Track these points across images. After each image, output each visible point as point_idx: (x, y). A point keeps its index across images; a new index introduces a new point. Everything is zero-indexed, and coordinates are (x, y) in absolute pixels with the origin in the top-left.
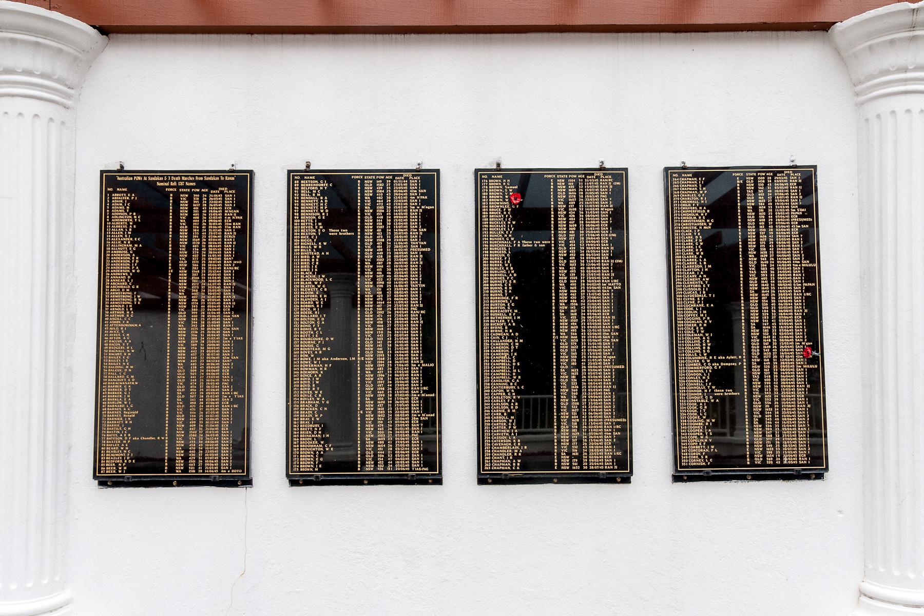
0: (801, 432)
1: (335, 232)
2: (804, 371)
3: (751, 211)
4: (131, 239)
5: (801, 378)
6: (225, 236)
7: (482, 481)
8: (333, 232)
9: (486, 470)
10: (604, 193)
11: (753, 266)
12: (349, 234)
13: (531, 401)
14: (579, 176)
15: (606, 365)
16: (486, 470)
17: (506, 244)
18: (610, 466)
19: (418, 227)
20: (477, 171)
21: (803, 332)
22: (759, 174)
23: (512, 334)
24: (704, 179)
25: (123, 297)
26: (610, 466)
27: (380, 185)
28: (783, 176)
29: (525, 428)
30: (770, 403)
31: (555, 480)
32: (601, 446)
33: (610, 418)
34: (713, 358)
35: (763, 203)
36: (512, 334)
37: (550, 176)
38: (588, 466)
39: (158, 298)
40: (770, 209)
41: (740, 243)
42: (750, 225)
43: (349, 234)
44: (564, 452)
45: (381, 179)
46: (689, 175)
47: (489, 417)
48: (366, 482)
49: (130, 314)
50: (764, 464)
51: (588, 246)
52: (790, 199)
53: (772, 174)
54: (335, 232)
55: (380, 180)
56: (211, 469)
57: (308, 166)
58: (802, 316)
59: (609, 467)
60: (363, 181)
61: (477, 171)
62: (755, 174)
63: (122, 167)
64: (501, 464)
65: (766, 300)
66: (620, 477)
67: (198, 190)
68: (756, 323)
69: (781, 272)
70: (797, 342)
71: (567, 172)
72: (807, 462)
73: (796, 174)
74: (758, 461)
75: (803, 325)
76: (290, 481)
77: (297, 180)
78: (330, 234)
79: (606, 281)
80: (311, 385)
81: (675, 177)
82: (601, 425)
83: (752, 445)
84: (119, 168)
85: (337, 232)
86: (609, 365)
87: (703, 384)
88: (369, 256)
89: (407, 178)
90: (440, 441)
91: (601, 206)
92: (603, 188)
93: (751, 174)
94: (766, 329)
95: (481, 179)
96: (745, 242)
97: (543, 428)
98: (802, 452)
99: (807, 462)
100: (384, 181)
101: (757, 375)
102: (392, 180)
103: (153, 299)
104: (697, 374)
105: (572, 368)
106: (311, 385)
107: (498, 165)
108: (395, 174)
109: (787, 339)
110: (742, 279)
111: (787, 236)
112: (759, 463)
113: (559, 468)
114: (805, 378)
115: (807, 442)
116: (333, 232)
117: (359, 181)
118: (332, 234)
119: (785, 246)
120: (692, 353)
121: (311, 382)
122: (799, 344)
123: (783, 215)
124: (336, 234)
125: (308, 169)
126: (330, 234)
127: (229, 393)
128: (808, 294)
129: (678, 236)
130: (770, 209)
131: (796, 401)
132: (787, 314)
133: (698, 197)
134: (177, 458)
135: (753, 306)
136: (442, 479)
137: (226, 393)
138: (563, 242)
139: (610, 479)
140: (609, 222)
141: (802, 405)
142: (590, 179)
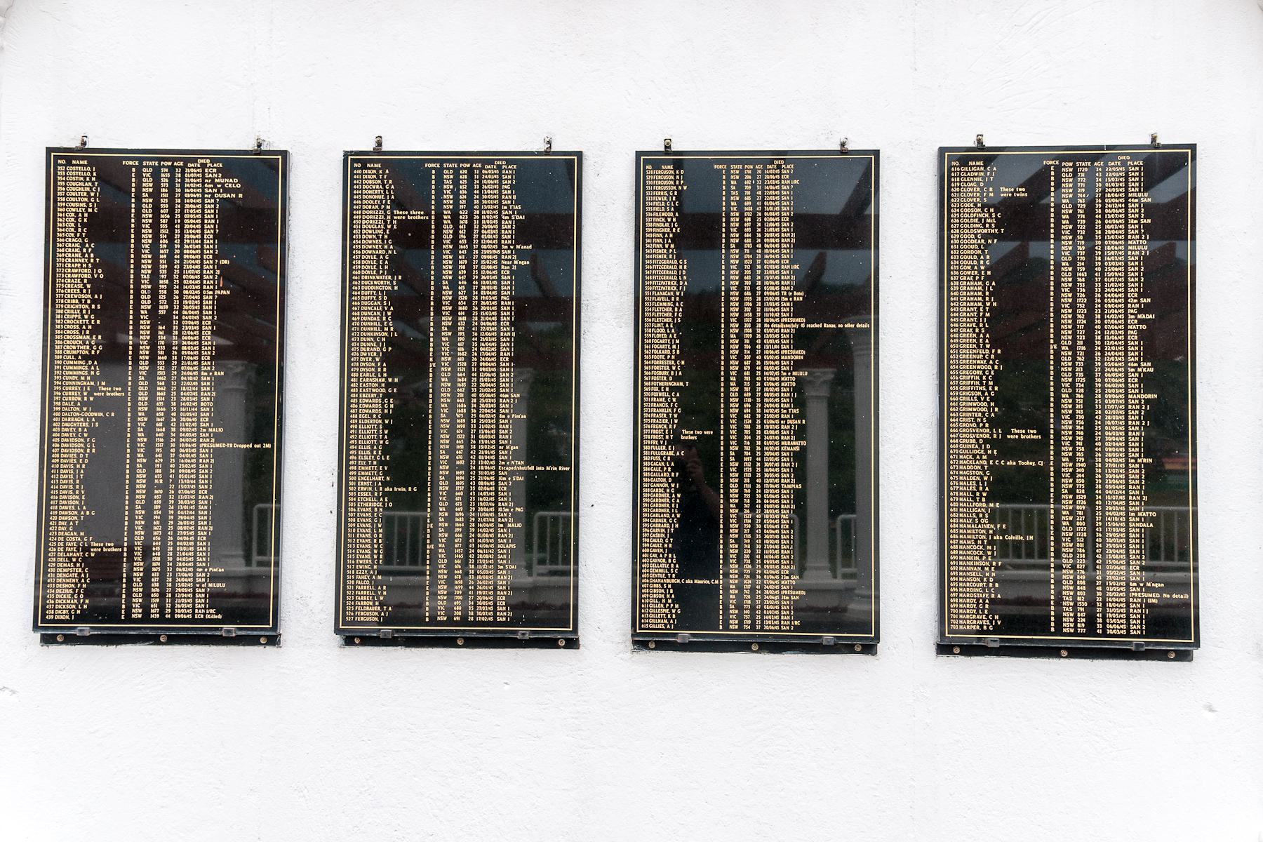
14: (474, 166)
20: (942, 151)
22: (162, 163)
24: (387, 171)
25: (76, 340)
27: (165, 176)
29: (410, 564)
31: (755, 647)
37: (130, 163)
38: (762, 625)
39: (228, 343)
45: (167, 167)
46: (82, 162)
49: (95, 371)
53: (182, 164)
55: (465, 169)
57: (84, 143)
60: (1058, 169)
61: (942, 151)
62: (157, 164)
63: (980, 142)
71: (460, 158)
72: (1142, 633)
73: (215, 165)
77: (61, 165)
80: (75, 481)
81: (61, 165)
84: (662, 149)
89: (499, 167)
90: (277, 578)
99: (1142, 633)
100: (172, 169)
102: (183, 169)
103: (225, 346)
104: (971, 478)
105: (457, 470)
106: (75, 481)
107: (1154, 139)
108: (187, 157)
113: (726, 628)
117: (134, 170)
121: (75, 476)
125: (83, 148)
134: (731, 587)
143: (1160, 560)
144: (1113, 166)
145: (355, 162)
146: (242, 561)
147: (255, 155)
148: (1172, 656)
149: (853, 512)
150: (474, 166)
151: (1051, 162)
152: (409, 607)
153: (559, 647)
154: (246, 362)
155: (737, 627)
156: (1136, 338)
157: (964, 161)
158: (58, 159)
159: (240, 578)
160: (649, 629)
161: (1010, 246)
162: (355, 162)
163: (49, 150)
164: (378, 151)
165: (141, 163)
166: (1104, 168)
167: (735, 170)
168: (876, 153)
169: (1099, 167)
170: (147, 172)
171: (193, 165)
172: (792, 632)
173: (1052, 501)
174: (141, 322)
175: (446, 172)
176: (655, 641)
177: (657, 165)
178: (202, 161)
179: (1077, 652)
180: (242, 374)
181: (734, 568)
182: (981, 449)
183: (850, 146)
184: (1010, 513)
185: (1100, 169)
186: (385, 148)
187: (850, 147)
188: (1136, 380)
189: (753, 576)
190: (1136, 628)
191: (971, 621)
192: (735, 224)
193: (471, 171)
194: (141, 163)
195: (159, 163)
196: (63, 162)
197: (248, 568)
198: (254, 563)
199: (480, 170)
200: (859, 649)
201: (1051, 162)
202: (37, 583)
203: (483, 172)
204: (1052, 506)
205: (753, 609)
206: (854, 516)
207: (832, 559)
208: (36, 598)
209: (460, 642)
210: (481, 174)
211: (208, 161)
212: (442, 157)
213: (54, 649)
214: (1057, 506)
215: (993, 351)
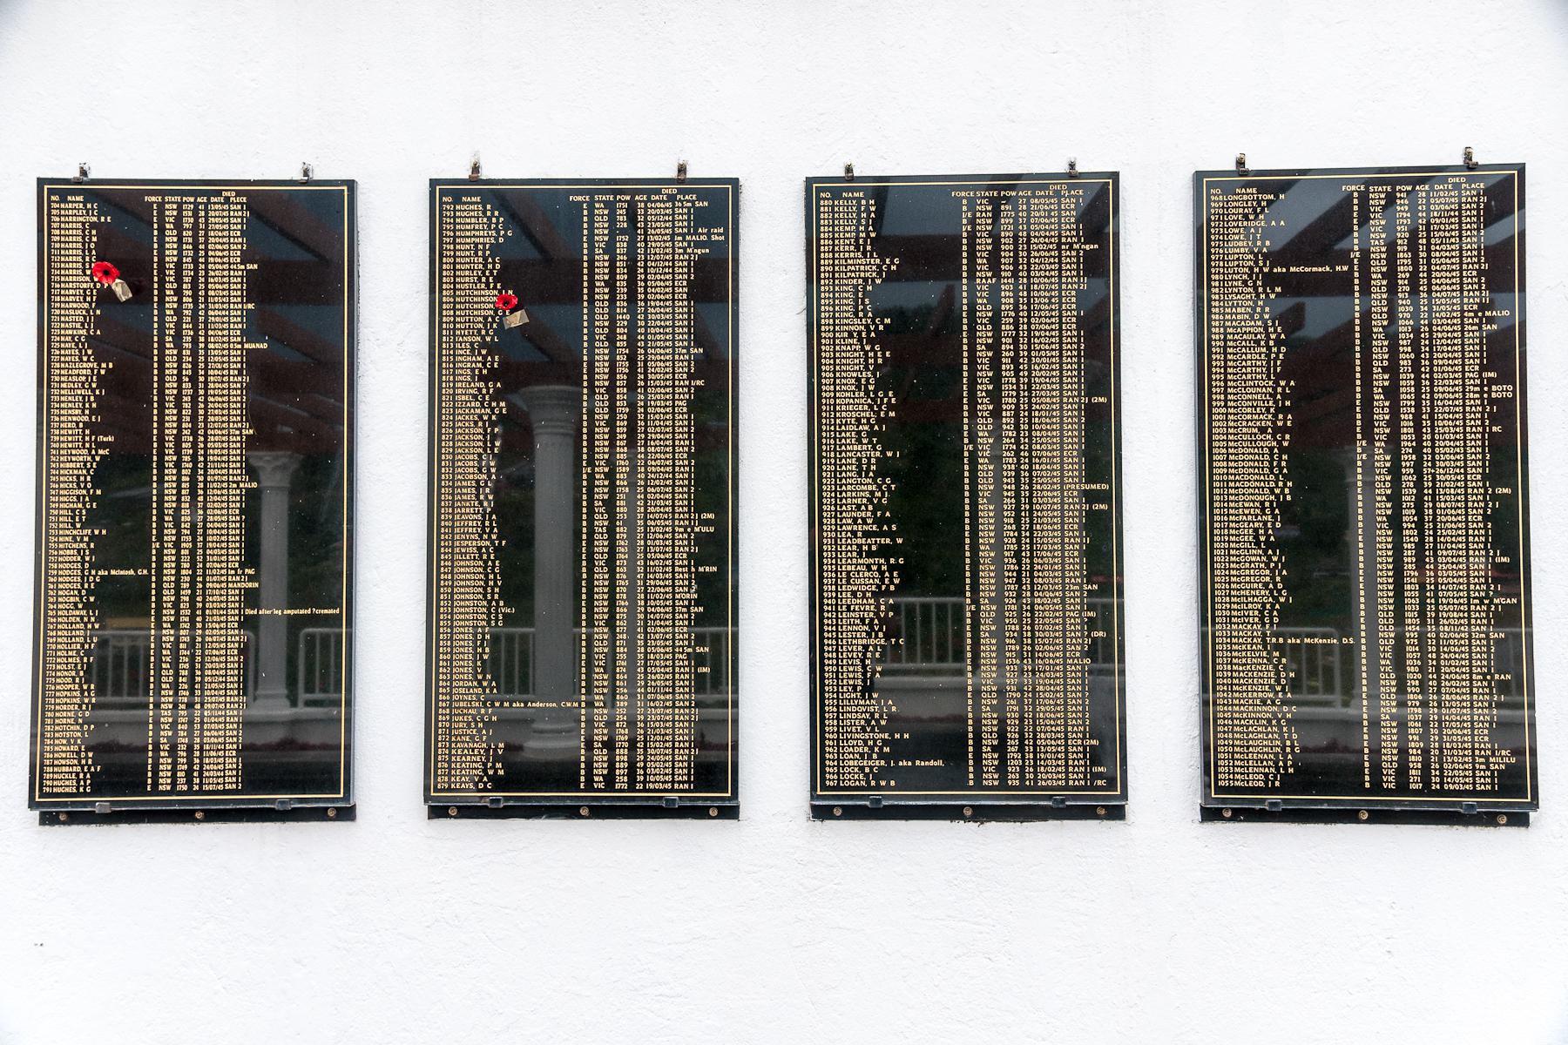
0: (1476, 566)
2: (1492, 777)
3: (1382, 397)
5: (1471, 224)
10: (1072, 607)
11: (1390, 772)
13: (918, 608)
14: (637, 198)
15: (1070, 483)
18: (1079, 780)
21: (1484, 460)
23: (876, 428)
26: (1079, 780)
28: (1449, 190)
29: (113, 695)
30: (1419, 663)
32: (1054, 257)
33: (1076, 483)
35: (1417, 749)
36: (876, 428)
41: (1357, 322)
42: (1384, 625)
44: (983, 497)
47: (834, 654)
48: (713, 812)
50: (1402, 788)
51: (1035, 383)
52: (1465, 433)
58: (1485, 515)
59: (1077, 783)
60: (1364, 197)
61: (809, 182)
64: (849, 274)
65: (1410, 333)
66: (1367, 810)
67: (192, 200)
68: (1383, 387)
69: (1447, 676)
70: (1474, 598)
72: (1493, 787)
73: (1473, 186)
74: (1389, 782)
75: (1483, 446)
76: (430, 807)
79: (1069, 240)
82: (1060, 712)
83: (1375, 724)
86: (1076, 483)
87: (1271, 395)
90: (349, 721)
91: (1063, 240)
92: (1071, 645)
93: (1380, 189)
94: (1410, 542)
95: (819, 199)
96: (1366, 316)
97: (943, 662)
98: (1471, 361)
99: (1493, 787)
101: (1379, 240)
109: (1451, 515)
110: (1359, 423)
111: (1458, 471)
112: (1391, 786)
114: (1481, 351)
115: (1487, 574)
119: (1451, 403)
120: (1251, 441)
122: (1480, 677)
123: (1450, 454)
128: (1494, 429)
129: (1219, 287)
131: (1461, 257)
133: (1268, 568)
135: (1384, 625)
136: (738, 807)
141: (1478, 502)
143: (947, 661)
145: (818, 192)
146: (287, 703)
149: (532, 625)
150: (637, 198)
151: (1353, 188)
152: (314, 747)
154: (289, 453)
156: (685, 410)
157: (457, 196)
158: (51, 192)
159: (283, 723)
162: (818, 192)
164: (474, 180)
165: (592, 198)
166: (206, 205)
168: (1115, 176)
170: (600, 210)
171: (657, 198)
174: (167, 411)
177: (457, 196)
178: (1453, 180)
180: (284, 468)
181: (167, 697)
183: (1081, 168)
184: (934, 608)
186: (690, 174)
187: (1079, 169)
188: (685, 456)
189: (190, 706)
191: (64, 781)
192: (602, 274)
194: (592, 198)
197: (294, 710)
198: (300, 703)
199: (206, 205)
201: (1353, 188)
202: (33, 736)
203: (649, 205)
205: (190, 749)
206: (532, 630)
207: (291, 681)
208: (33, 755)
210: (646, 209)
211: (1463, 180)
215: (93, 438)
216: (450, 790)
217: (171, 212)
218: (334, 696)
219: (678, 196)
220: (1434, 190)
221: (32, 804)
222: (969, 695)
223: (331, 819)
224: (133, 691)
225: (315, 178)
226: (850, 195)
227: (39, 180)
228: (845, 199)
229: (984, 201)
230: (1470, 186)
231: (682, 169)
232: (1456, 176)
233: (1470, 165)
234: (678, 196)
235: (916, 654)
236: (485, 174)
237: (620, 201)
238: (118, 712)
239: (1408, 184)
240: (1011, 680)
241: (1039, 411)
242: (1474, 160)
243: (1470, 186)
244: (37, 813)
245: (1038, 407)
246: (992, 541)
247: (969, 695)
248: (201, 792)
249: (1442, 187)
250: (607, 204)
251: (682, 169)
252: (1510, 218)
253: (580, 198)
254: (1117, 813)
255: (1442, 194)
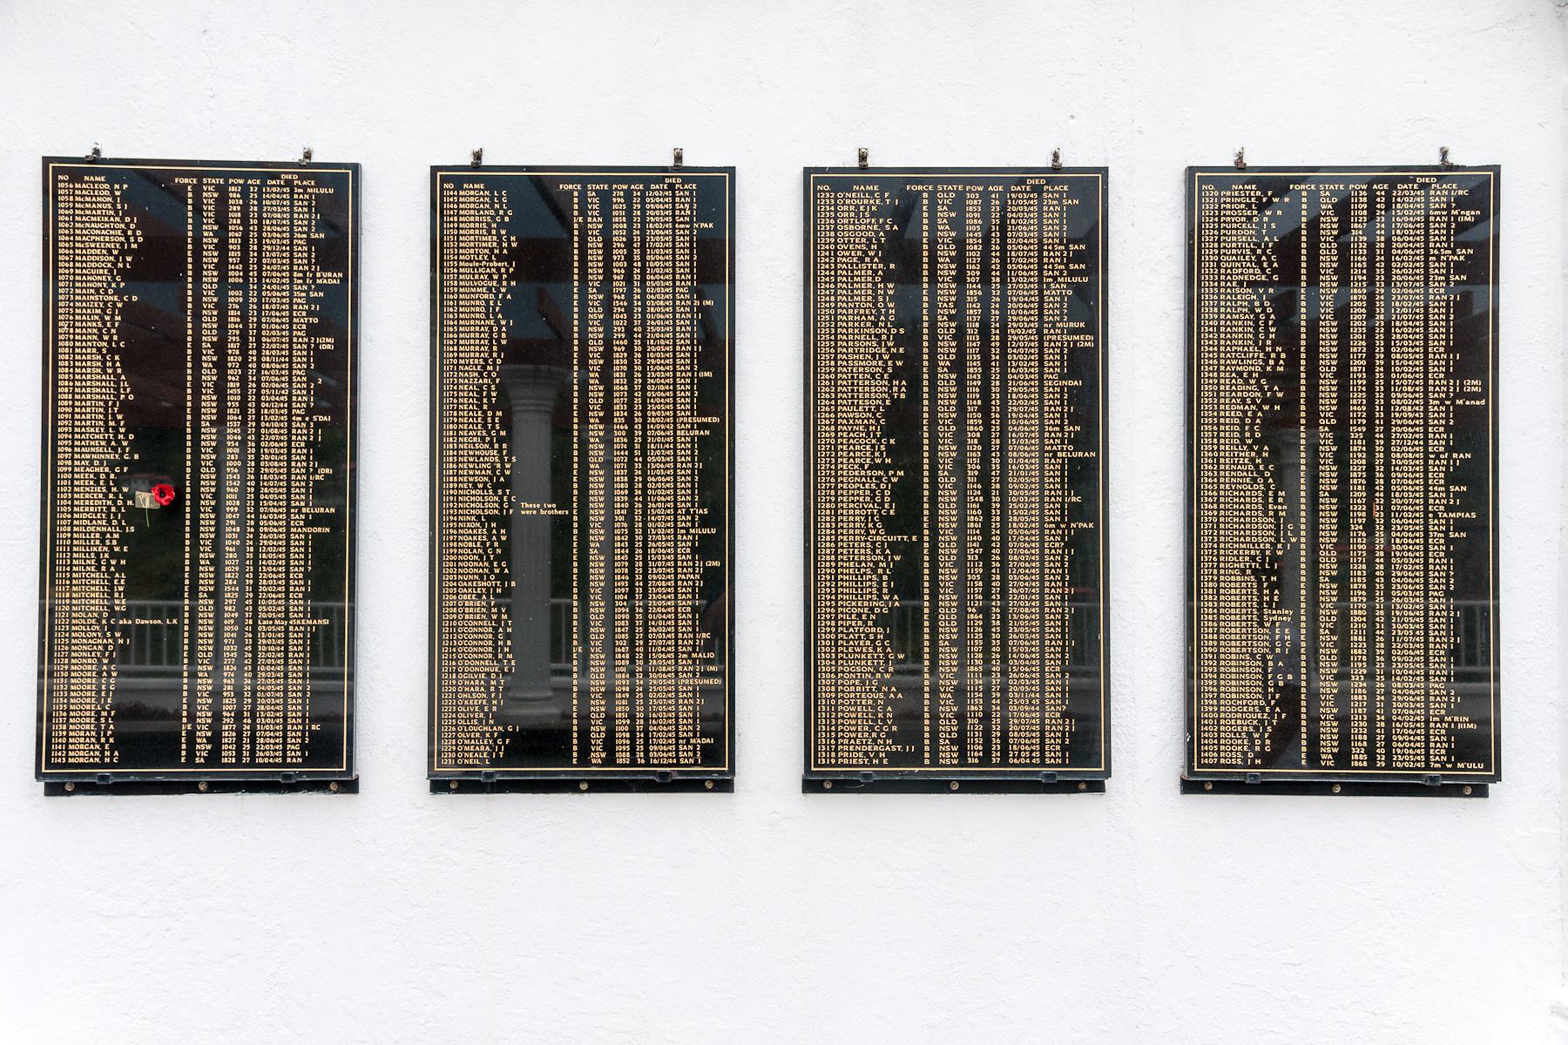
1: (533, 509)
4: (501, 728)
6: (1046, 544)
7: (812, 785)
8: (529, 509)
9: (1205, 766)
12: (560, 512)
16: (1205, 766)
17: (105, 394)
19: (1062, 422)
29: (324, 665)
34: (130, 298)
40: (995, 515)
43: (560, 512)
54: (533, 509)
56: (1408, 758)
61: (1191, 171)
63: (97, 151)
71: (227, 171)
73: (686, 187)
78: (523, 512)
85: (536, 509)
88: (209, 336)
93: (950, 187)
95: (56, 181)
105: (231, 290)
108: (266, 172)
116: (529, 509)
118: (527, 512)
124: (535, 512)
125: (96, 158)
126: (523, 512)
127: (307, 268)
130: (995, 515)
132: (1411, 245)
137: (301, 268)
138: (209, 385)
139: (692, 785)
140: (306, 569)
142: (1019, 192)
144: (274, 186)
145: (445, 181)
147: (90, 162)
148: (1469, 791)
150: (249, 182)
153: (706, 790)
155: (1365, 764)
157: (459, 183)
160: (1404, 768)
161: (1284, 290)
162: (445, 181)
163: (46, 161)
166: (260, 187)
167: (946, 197)
169: (637, 191)
171: (274, 182)
172: (1067, 766)
173: (186, 595)
175: (232, 189)
176: (1212, 782)
177: (459, 183)
178: (286, 177)
179: (600, 786)
182: (483, 527)
185: (639, 194)
190: (294, 755)
191: (82, 750)
193: (628, 196)
195: (610, 187)
196: (66, 178)
200: (828, 786)
204: (187, 602)
209: (584, 786)
212: (201, 170)
213: (444, 798)
214: (193, 603)
216: (1218, 765)
217: (210, 195)
218: (337, 669)
219: (1045, 188)
220: (266, 185)
221: (39, 775)
222: (574, 695)
223: (827, 791)
224: (329, 662)
225: (108, 157)
226: (862, 187)
227: (44, 158)
228: (856, 191)
229: (211, 188)
230: (1441, 186)
231: (478, 156)
232: (672, 177)
233: (1240, 166)
234: (1045, 188)
235: (130, 659)
236: (486, 161)
237: (233, 184)
238: (156, 680)
239: (240, 178)
240: (622, 681)
241: (269, 409)
242: (1060, 161)
243: (1441, 186)
244: (43, 784)
245: (267, 405)
246: (602, 538)
247: (574, 695)
248: (252, 764)
249: (657, 187)
250: (218, 188)
251: (478, 156)
252: (1486, 223)
253: (186, 181)
254: (725, 786)
255: (657, 193)
